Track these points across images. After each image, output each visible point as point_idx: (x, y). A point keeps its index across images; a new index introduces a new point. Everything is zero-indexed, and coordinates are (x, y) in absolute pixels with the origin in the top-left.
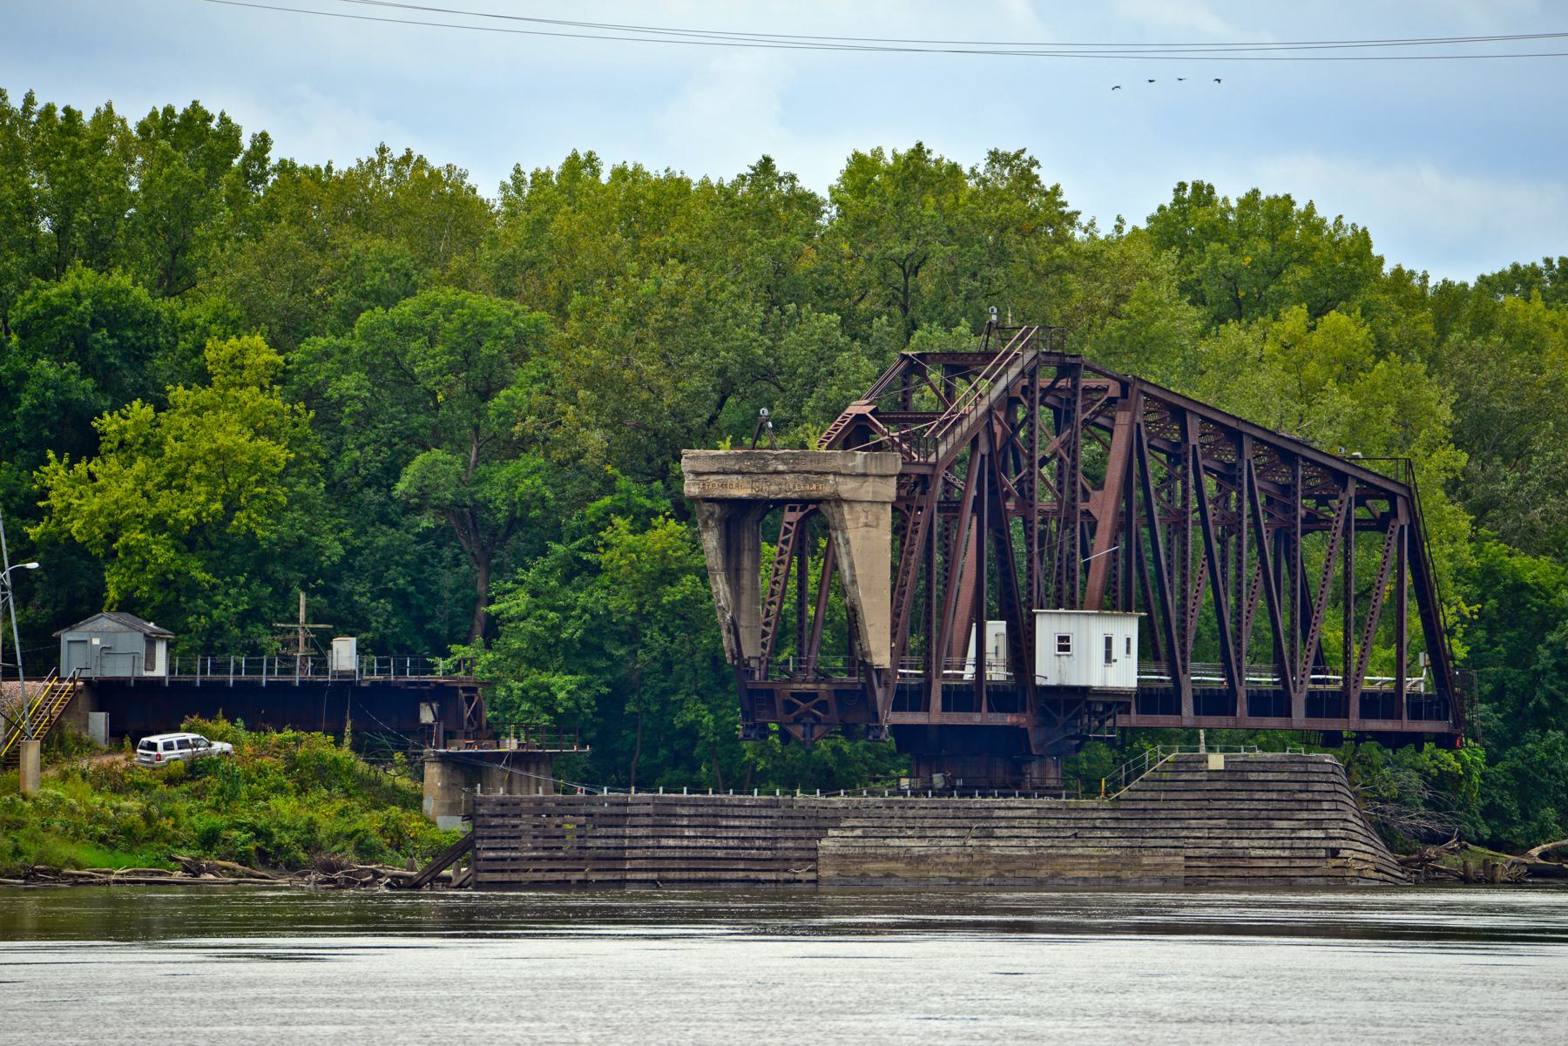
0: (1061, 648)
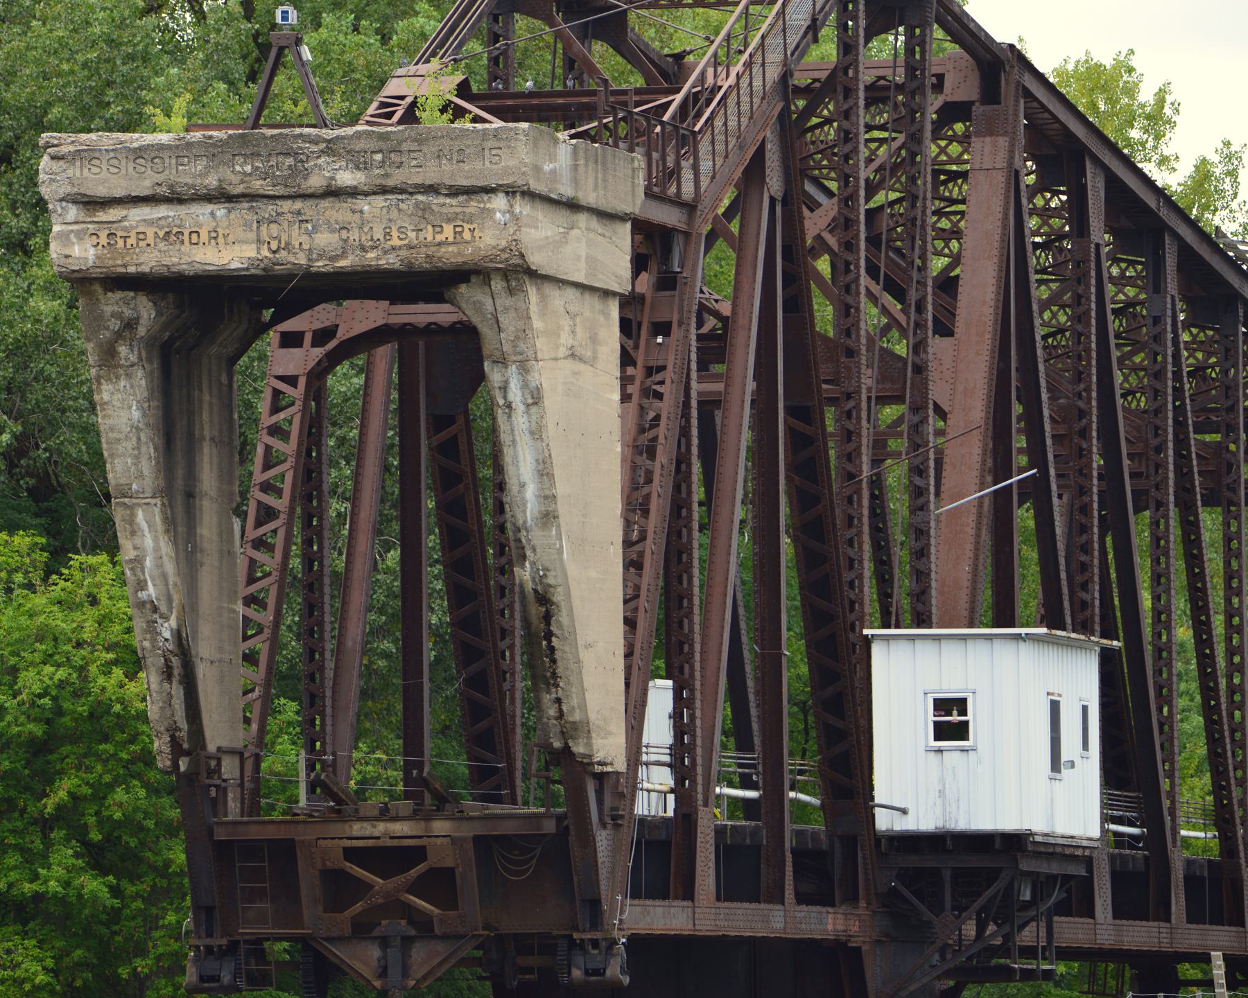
0: (944, 732)
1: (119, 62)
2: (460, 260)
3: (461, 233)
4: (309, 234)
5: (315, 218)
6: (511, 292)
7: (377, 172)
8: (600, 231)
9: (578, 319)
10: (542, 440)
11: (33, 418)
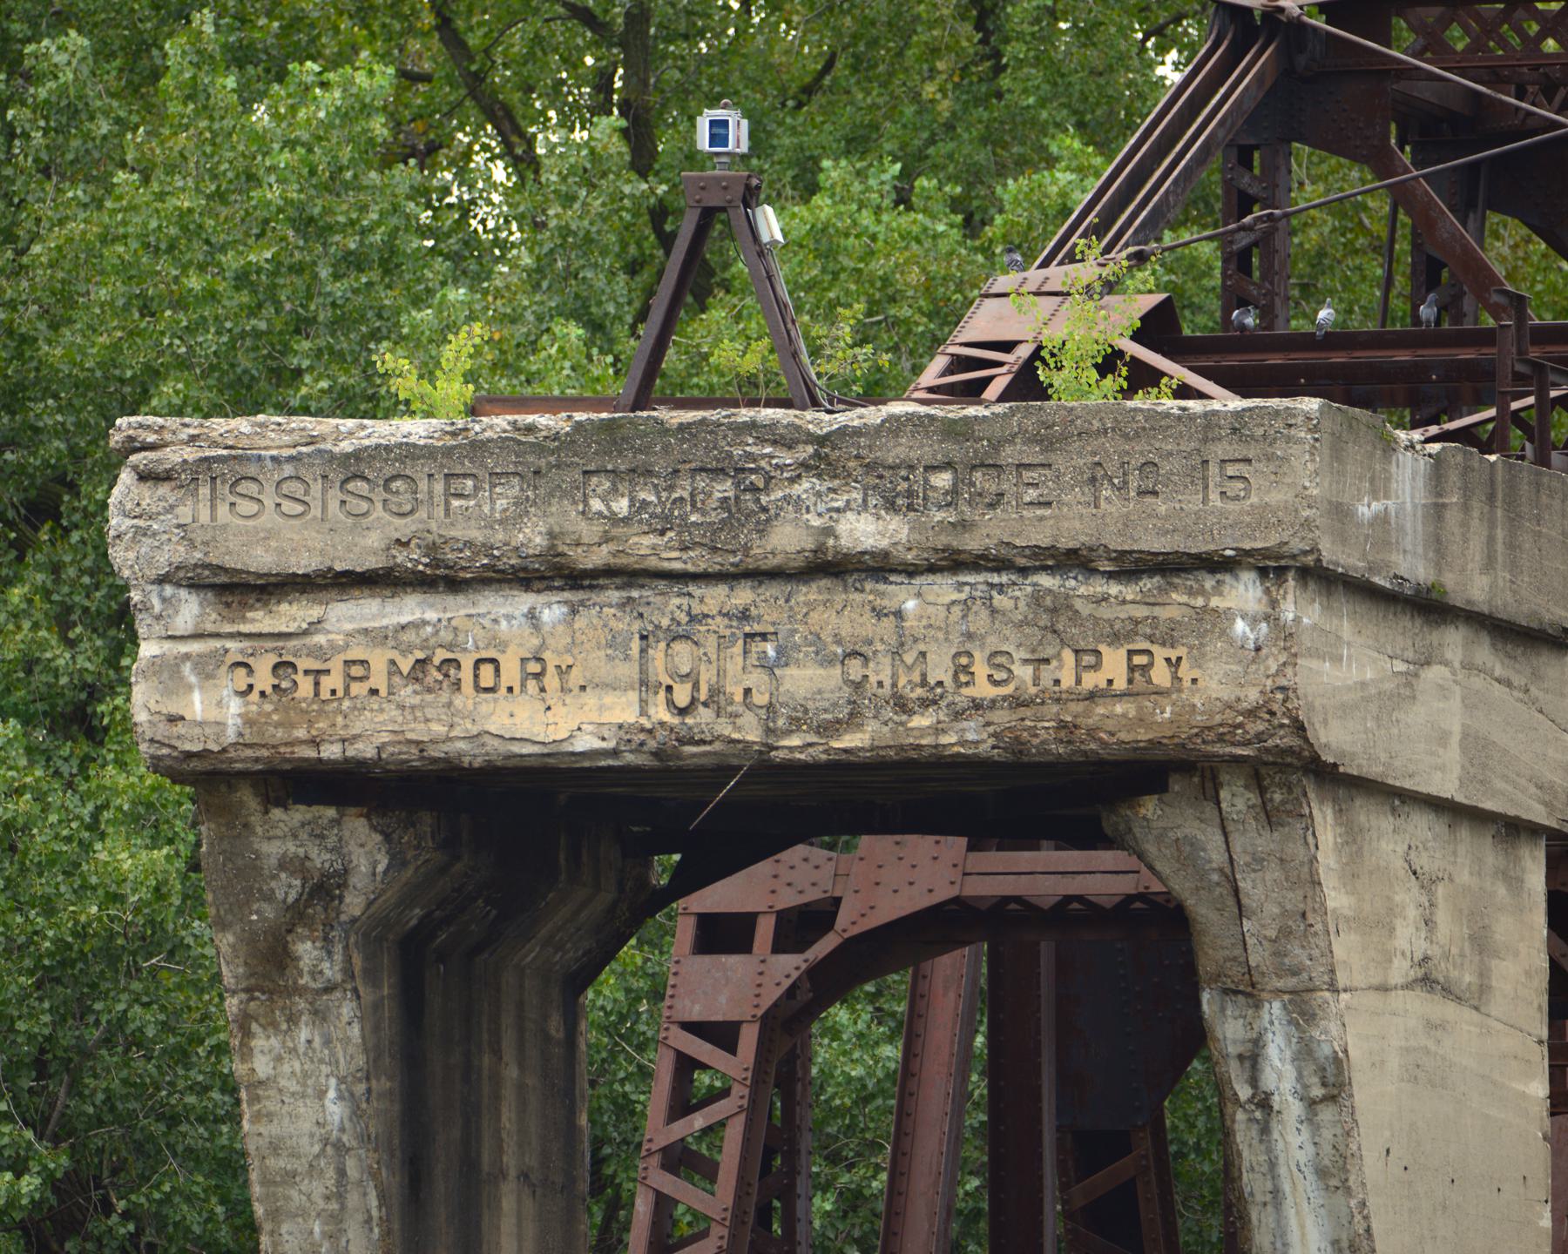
1: (324, 273)
2: (1143, 735)
3: (1145, 669)
4: (768, 667)
5: (783, 629)
6: (1270, 817)
7: (939, 516)
8: (1499, 671)
9: (1441, 890)
10: (1348, 1191)
11: (98, 1137)
